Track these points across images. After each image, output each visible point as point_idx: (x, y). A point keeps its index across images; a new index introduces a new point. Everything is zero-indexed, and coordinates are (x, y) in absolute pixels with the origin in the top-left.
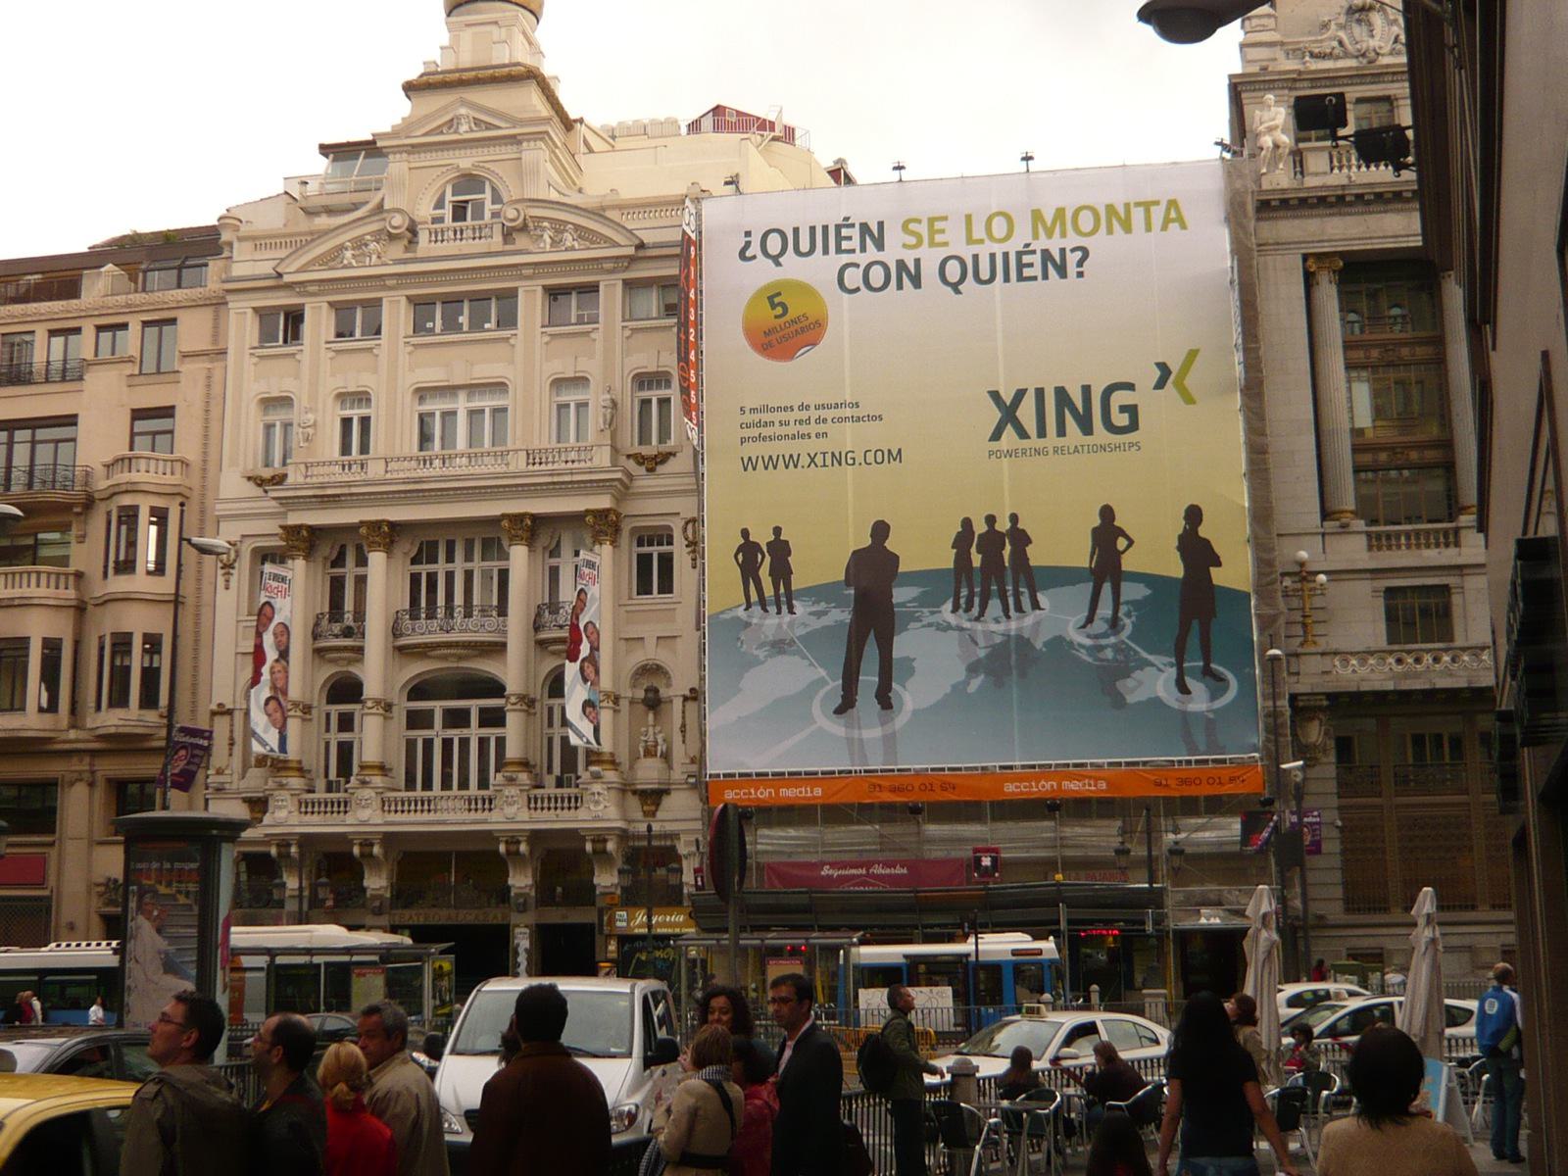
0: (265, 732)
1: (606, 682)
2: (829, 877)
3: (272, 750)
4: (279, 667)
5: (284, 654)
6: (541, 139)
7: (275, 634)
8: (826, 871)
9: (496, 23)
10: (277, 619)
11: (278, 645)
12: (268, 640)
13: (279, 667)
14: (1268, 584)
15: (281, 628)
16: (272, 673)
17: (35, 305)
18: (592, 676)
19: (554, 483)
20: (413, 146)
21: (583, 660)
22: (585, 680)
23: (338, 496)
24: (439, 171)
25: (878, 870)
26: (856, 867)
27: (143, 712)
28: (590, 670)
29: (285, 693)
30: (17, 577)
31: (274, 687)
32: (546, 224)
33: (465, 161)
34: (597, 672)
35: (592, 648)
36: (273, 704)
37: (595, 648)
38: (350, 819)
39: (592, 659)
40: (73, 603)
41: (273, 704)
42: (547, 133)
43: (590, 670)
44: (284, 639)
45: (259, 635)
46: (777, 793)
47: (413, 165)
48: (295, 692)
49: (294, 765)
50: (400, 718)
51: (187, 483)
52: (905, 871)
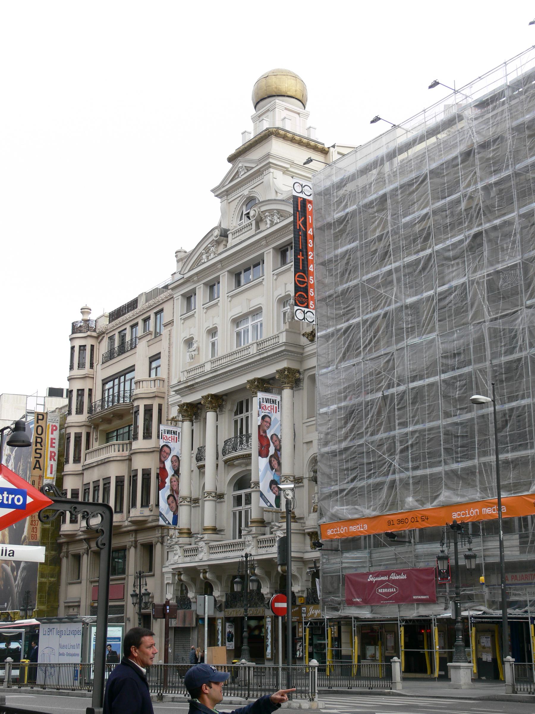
0: (167, 513)
1: (286, 469)
2: (371, 582)
3: (169, 523)
4: (174, 479)
5: (177, 472)
6: (270, 167)
7: (172, 461)
8: (371, 579)
9: (299, 114)
10: (173, 454)
11: (173, 467)
12: (168, 465)
13: (174, 479)
14: (462, 337)
15: (175, 458)
16: (171, 482)
17: (122, 317)
18: (276, 466)
19: (263, 359)
20: (227, 191)
21: (271, 456)
22: (272, 468)
23: (192, 385)
24: (237, 200)
25: (394, 577)
26: (383, 575)
27: (142, 509)
28: (275, 463)
29: (178, 493)
30: (125, 446)
31: (172, 490)
32: (267, 214)
33: (245, 191)
34: (279, 464)
35: (276, 450)
36: (171, 498)
37: (278, 449)
38: (197, 559)
39: (277, 456)
40: (127, 458)
41: (171, 498)
42: (270, 163)
43: (275, 463)
44: (177, 464)
45: (162, 462)
46: (348, 529)
47: (230, 201)
48: (184, 491)
49: (186, 531)
50: (229, 500)
51: (162, 390)
52: (405, 577)
